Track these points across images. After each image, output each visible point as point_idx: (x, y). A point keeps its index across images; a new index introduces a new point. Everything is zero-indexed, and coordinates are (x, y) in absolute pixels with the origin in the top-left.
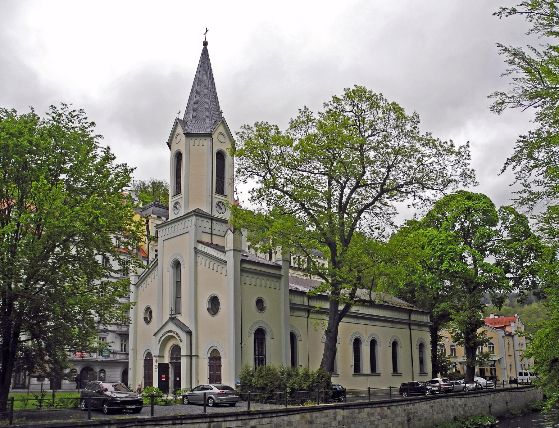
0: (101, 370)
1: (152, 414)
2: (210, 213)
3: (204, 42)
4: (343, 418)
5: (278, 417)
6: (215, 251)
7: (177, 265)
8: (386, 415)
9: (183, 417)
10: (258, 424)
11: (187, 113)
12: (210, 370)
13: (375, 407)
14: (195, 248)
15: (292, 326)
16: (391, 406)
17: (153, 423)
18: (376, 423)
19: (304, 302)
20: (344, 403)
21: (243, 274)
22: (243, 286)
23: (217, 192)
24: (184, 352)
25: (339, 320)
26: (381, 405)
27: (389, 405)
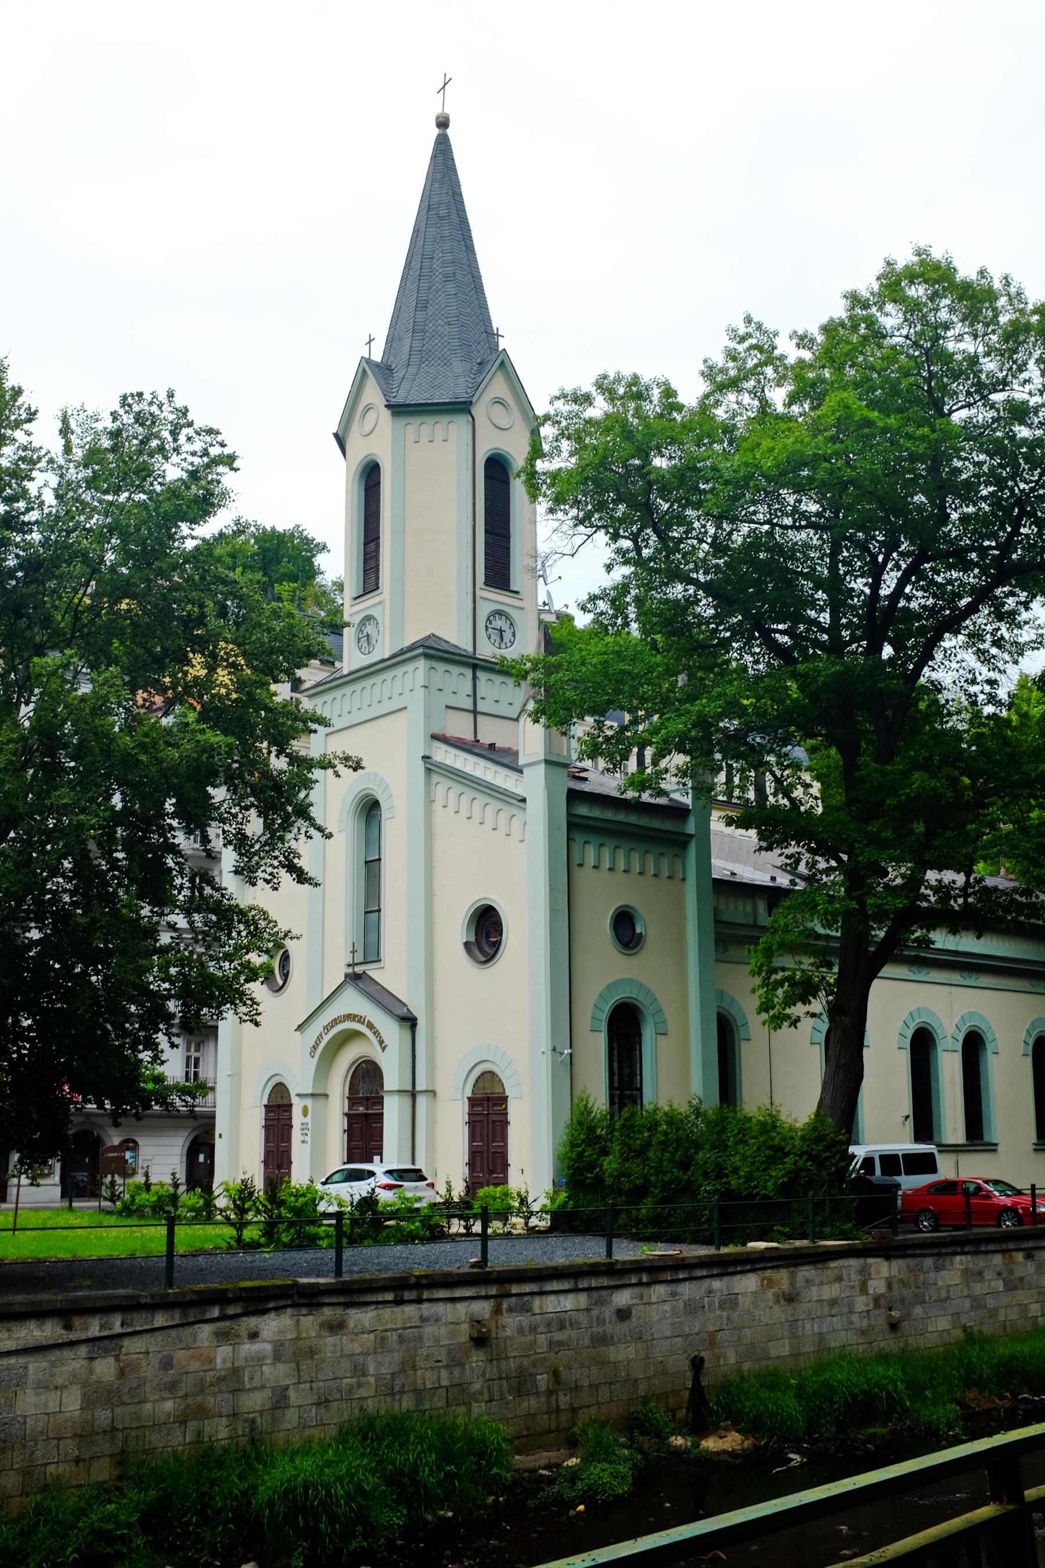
0: (127, 1141)
1: (338, 1272)
2: (470, 649)
3: (437, 118)
4: (889, 1286)
6: (489, 764)
8: (1021, 1279)
9: (424, 1282)
10: (635, 1301)
11: (390, 341)
12: (472, 1138)
13: (986, 1252)
14: (426, 758)
15: (721, 994)
17: (342, 1300)
18: (991, 1302)
19: (755, 917)
22: (576, 870)
24: (393, 1079)
26: (1004, 1247)
27: (1031, 1244)
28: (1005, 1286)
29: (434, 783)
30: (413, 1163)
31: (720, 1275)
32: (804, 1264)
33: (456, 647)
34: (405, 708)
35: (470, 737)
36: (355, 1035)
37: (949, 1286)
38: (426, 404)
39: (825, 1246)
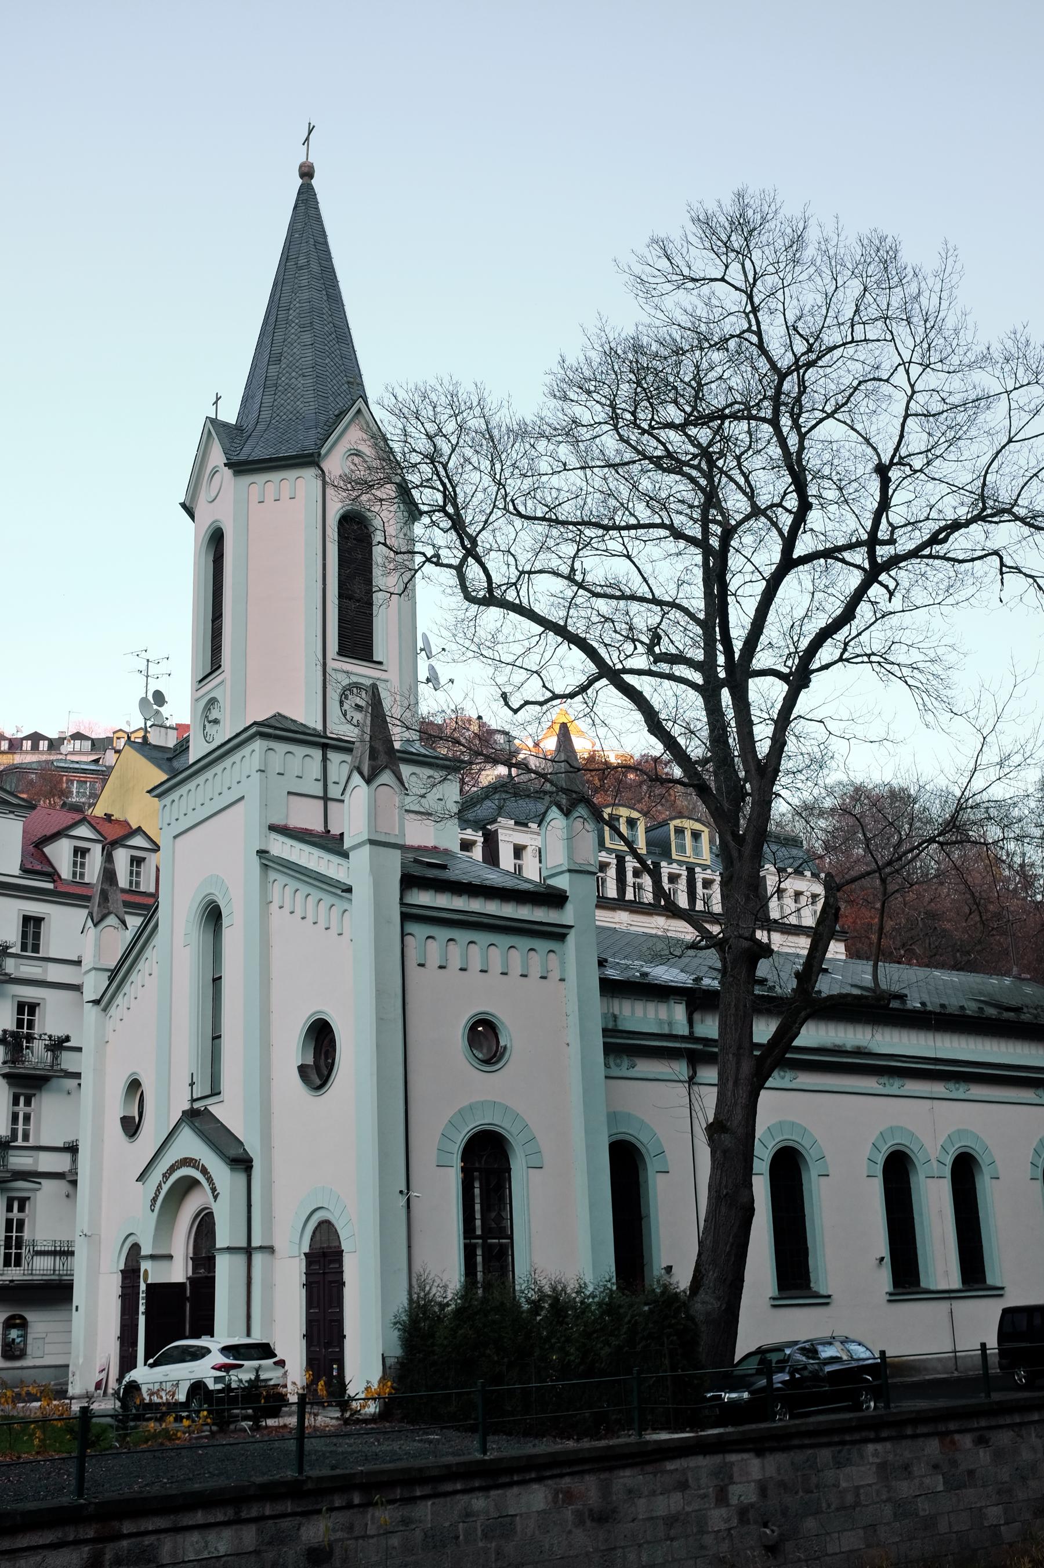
2: (319, 727)
3: (301, 167)
4: (763, 1489)
5: (441, 1500)
7: (213, 916)
8: (971, 1473)
10: (339, 1535)
13: (915, 1437)
14: (262, 853)
16: (989, 1428)
18: (924, 1508)
20: (1026, 1394)
21: (412, 928)
23: (344, 651)
25: (758, 1084)
26: (942, 1428)
27: (983, 1423)
28: (945, 1483)
29: (271, 881)
30: (249, 1334)
31: (485, 1489)
32: (624, 1467)
33: (304, 726)
34: (243, 798)
35: (319, 828)
36: (188, 1185)
37: (858, 1488)
38: (271, 460)
39: (656, 1442)
